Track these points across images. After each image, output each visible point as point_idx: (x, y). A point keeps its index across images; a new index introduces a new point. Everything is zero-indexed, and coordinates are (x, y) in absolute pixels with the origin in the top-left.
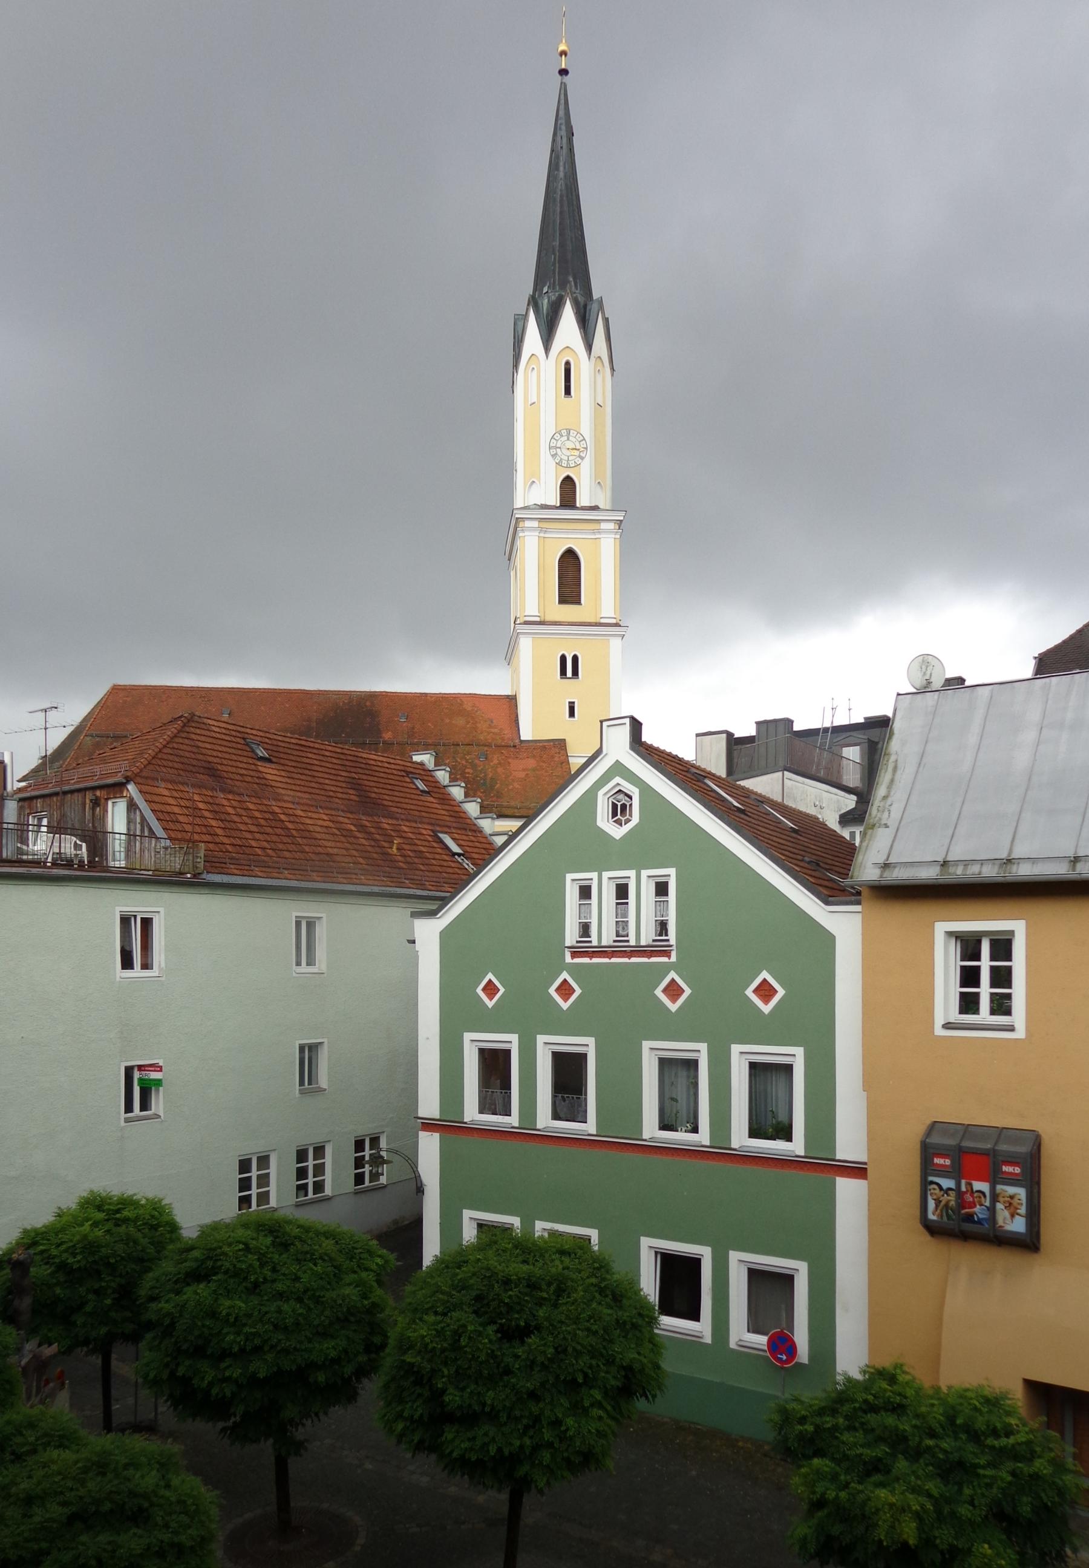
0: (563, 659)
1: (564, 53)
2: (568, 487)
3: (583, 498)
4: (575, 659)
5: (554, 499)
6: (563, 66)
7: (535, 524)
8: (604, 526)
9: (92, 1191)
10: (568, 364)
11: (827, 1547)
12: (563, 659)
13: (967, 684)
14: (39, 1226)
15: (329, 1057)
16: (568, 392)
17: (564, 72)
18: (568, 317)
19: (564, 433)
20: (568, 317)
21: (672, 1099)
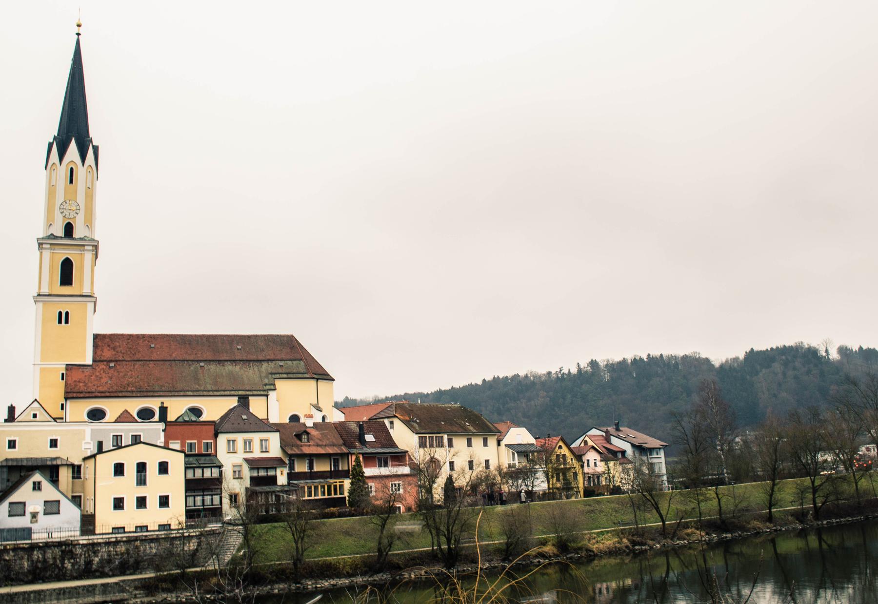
0: (60, 313)
2: (69, 230)
3: (78, 233)
4: (67, 313)
5: (60, 232)
7: (48, 246)
8: (86, 248)
9: (593, 364)
10: (72, 169)
12: (60, 313)
13: (203, 418)
14: (371, 400)
16: (71, 182)
18: (73, 147)
20: (73, 147)
21: (471, 467)
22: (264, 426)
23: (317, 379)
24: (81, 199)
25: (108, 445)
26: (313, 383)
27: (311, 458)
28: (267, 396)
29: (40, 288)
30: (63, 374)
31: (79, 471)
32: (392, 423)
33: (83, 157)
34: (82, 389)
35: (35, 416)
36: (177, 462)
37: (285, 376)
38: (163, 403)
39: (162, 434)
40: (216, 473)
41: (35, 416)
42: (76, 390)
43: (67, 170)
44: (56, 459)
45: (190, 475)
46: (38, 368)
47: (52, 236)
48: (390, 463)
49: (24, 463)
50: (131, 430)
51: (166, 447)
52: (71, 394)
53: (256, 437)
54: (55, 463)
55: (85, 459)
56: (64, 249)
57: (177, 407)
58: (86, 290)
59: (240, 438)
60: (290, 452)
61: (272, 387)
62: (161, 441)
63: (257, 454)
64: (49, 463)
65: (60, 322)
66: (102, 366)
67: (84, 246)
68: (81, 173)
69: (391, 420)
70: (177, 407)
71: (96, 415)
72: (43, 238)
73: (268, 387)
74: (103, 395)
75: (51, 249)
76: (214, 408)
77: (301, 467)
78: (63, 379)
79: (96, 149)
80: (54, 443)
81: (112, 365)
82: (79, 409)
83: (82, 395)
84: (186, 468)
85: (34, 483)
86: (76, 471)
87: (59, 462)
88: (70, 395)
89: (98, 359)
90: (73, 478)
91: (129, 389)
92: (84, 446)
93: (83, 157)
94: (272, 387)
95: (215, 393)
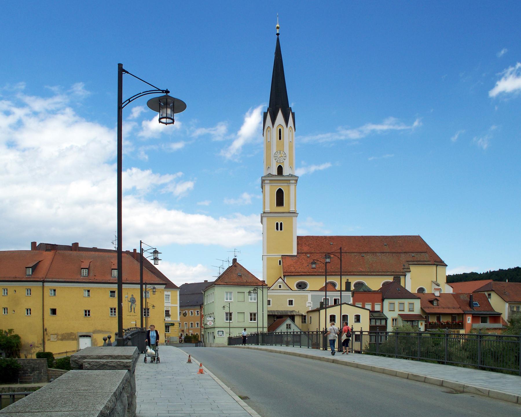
0: (277, 224)
1: (278, 28)
2: (280, 169)
3: (286, 172)
4: (281, 224)
5: (275, 172)
6: (278, 32)
7: (268, 182)
8: (291, 182)
10: (280, 130)
11: (10, 344)
12: (277, 224)
15: (108, 362)
16: (280, 138)
17: (278, 34)
18: (280, 116)
19: (279, 152)
20: (280, 116)
22: (406, 295)
23: (437, 265)
24: (286, 150)
25: (331, 302)
26: (434, 267)
27: (439, 315)
28: (405, 275)
29: (264, 208)
30: (280, 261)
31: (305, 319)
32: (489, 295)
33: (287, 121)
34: (293, 270)
35: (280, 286)
36: (365, 316)
37: (415, 263)
38: (348, 280)
39: (352, 298)
40: (383, 323)
41: (280, 286)
42: (289, 270)
43: (277, 131)
44: (292, 311)
45: (373, 324)
46: (265, 257)
47: (270, 175)
48: (488, 320)
49: (276, 314)
50: (334, 296)
51: (353, 305)
52: (287, 274)
53: (406, 302)
54: (292, 314)
55: (308, 312)
56: (283, 183)
57: (354, 280)
58: (292, 209)
59: (397, 302)
60: (427, 311)
61: (408, 270)
62: (351, 302)
63: (406, 312)
64: (289, 314)
65: (277, 229)
66: (303, 256)
67: (290, 180)
68: (286, 132)
69: (489, 293)
70: (354, 280)
71: (301, 286)
72: (265, 177)
73: (405, 270)
74: (305, 274)
75: (270, 183)
76: (375, 283)
77: (433, 320)
78: (280, 264)
79: (293, 114)
80: (291, 302)
81: (309, 255)
82: (293, 282)
83: (293, 274)
84: (370, 319)
85: (287, 325)
86: (304, 317)
87: (295, 314)
88: (287, 274)
89: (300, 252)
90: (166, 331)
91: (320, 270)
92: (308, 305)
93: (287, 121)
94: (408, 270)
95: (372, 273)
